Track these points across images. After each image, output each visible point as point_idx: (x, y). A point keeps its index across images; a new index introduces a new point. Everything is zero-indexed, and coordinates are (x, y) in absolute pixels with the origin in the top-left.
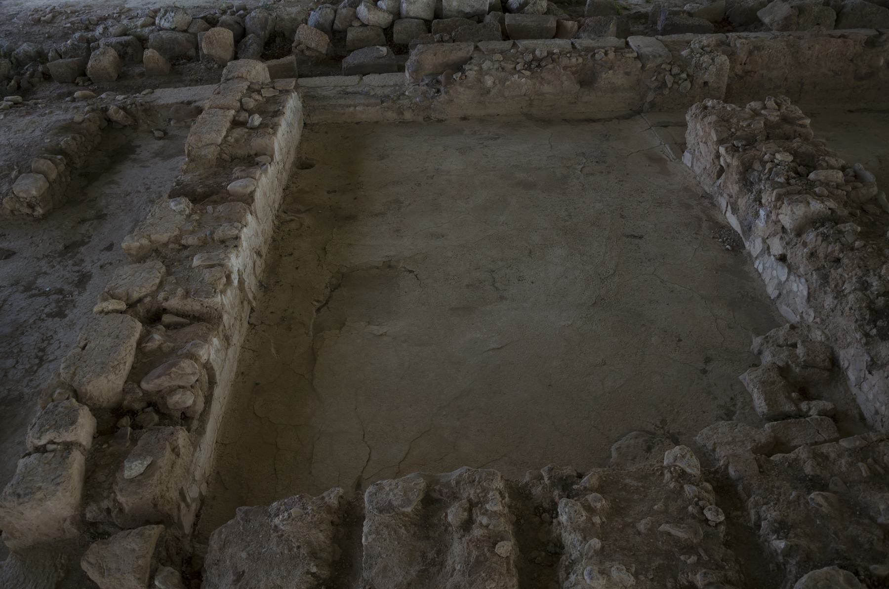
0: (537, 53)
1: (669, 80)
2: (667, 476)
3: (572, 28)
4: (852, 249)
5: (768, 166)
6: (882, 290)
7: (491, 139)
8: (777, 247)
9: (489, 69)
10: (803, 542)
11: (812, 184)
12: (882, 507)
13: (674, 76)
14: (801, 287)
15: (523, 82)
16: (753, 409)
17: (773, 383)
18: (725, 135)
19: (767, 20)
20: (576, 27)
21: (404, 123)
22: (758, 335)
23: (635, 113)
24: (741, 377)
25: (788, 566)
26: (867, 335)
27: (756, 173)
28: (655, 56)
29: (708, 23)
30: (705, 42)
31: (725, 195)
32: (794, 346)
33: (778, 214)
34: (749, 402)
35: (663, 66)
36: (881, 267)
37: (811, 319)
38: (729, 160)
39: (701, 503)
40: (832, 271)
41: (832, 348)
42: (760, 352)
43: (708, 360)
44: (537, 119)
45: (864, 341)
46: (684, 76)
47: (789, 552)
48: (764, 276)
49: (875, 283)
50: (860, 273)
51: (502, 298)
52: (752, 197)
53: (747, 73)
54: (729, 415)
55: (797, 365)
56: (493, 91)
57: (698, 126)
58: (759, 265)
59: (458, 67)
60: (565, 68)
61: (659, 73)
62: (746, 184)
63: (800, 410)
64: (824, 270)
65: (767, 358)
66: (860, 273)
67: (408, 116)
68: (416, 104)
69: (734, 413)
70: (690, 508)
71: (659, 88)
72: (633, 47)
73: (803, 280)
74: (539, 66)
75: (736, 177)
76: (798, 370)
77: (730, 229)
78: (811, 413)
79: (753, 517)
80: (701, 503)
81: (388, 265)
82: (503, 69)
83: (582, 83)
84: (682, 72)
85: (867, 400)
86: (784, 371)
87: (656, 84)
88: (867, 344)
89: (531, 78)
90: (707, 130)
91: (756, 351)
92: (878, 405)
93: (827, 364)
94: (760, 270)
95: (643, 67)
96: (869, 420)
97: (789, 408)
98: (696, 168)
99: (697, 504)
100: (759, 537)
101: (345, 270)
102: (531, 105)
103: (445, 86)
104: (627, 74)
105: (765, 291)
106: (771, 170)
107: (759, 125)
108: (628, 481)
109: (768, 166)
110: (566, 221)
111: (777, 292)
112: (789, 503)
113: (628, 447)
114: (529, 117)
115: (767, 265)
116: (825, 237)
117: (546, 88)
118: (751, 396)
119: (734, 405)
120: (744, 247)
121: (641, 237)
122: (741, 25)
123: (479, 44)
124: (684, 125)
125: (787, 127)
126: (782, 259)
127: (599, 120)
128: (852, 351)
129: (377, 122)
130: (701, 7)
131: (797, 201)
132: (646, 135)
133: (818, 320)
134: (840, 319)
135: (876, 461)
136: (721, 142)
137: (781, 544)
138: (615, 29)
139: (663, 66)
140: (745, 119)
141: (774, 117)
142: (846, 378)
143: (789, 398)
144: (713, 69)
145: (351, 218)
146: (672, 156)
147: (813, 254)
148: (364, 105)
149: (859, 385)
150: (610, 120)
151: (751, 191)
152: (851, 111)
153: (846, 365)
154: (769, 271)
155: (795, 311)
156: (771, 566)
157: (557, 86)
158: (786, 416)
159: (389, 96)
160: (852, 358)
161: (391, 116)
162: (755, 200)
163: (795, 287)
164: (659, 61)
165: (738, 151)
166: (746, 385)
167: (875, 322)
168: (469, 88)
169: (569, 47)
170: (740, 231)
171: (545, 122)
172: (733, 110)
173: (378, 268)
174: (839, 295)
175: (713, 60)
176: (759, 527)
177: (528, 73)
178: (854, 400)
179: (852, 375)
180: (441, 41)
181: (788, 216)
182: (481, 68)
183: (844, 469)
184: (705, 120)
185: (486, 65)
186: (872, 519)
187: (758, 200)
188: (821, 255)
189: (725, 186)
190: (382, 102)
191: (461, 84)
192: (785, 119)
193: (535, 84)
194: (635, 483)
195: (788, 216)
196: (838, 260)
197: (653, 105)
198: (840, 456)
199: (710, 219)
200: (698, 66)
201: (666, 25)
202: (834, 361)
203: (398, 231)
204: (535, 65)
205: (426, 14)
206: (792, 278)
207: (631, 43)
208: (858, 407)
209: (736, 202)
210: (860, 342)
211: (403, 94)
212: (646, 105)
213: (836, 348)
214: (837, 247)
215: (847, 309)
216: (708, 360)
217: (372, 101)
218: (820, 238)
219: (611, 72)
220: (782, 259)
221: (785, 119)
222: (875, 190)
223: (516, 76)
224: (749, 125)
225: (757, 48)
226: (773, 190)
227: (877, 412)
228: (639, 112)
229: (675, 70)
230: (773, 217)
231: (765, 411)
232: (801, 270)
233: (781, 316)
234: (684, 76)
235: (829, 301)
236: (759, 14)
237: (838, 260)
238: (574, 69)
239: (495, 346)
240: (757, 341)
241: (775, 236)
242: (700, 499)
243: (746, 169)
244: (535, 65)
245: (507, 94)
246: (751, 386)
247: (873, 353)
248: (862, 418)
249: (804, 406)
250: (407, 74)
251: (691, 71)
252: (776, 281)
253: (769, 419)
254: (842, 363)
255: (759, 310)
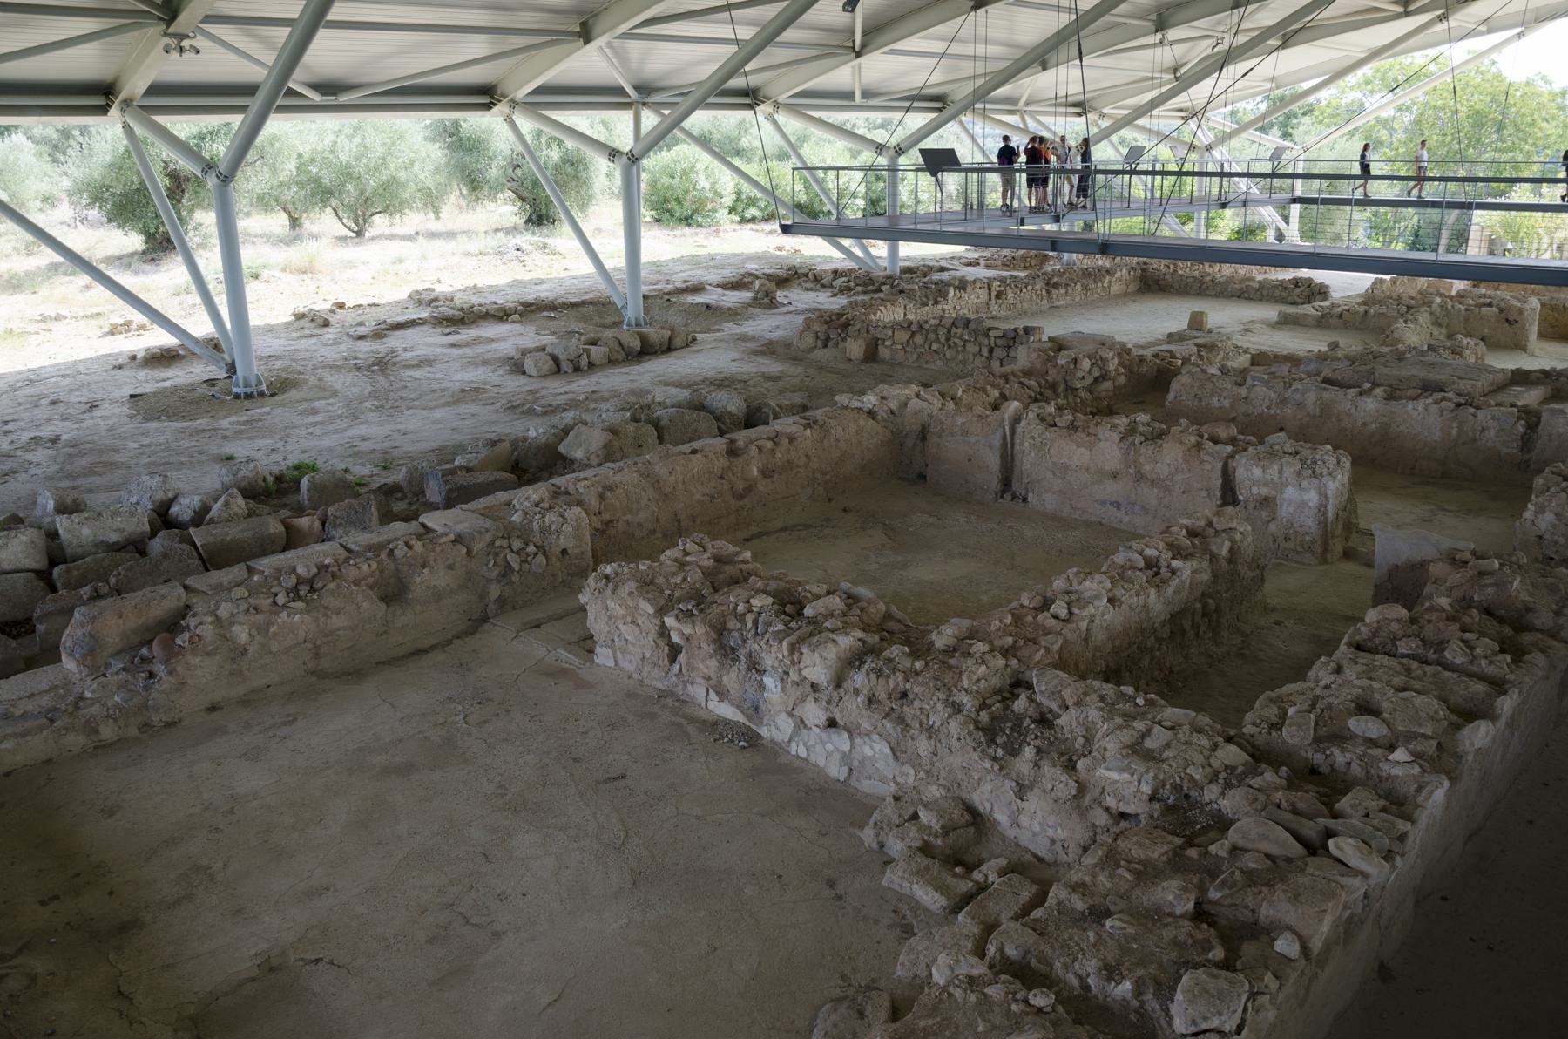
0: (300, 570)
1: (514, 560)
2: (958, 993)
3: (311, 526)
4: (917, 673)
5: (749, 618)
6: (977, 703)
7: (284, 724)
8: (814, 713)
9: (232, 615)
10: (1141, 972)
11: (813, 621)
12: (1171, 898)
13: (517, 553)
14: (877, 747)
15: (297, 621)
16: (926, 910)
17: (928, 869)
18: (662, 602)
19: (579, 454)
20: (317, 524)
21: (104, 748)
22: (862, 828)
23: (479, 622)
24: (884, 883)
25: (1147, 1006)
26: (995, 759)
27: (736, 634)
28: (480, 533)
29: (505, 475)
30: (535, 497)
31: (698, 680)
32: (915, 817)
33: (800, 671)
34: (916, 906)
35: (498, 543)
36: (960, 679)
37: (912, 779)
38: (687, 630)
39: (1018, 996)
40: (905, 708)
41: (959, 797)
42: (882, 845)
43: (831, 884)
44: (337, 673)
45: (996, 767)
46: (531, 549)
47: (1138, 992)
48: (813, 759)
49: (967, 702)
50: (942, 696)
51: (497, 935)
52: (743, 667)
53: (608, 523)
54: (908, 931)
55: (936, 837)
56: (251, 649)
57: (611, 604)
58: (797, 749)
59: (173, 625)
60: (356, 583)
61: (497, 554)
62: (726, 652)
63: (977, 883)
64: (893, 708)
65: (895, 846)
66: (942, 696)
67: (107, 732)
68: (117, 706)
69: (912, 926)
70: (1014, 1007)
71: (504, 575)
72: (435, 527)
73: (875, 737)
74: (312, 590)
75: (708, 648)
76: (939, 842)
77: (727, 722)
78: (991, 880)
79: (1075, 982)
80: (1018, 996)
81: (270, 967)
82: (256, 609)
83: (387, 599)
84: (527, 544)
85: (1034, 834)
86: (926, 850)
87: (496, 572)
88: (1001, 769)
89: (308, 612)
90: (630, 603)
91: (875, 846)
92: (1050, 832)
93: (968, 817)
94: (802, 752)
95: (469, 552)
96: (1048, 857)
97: (964, 886)
98: (624, 665)
99: (1016, 1000)
100: (1096, 997)
101: (191, 1010)
102: (317, 656)
103: (167, 662)
104: (450, 567)
105: (827, 776)
106: (755, 623)
107: (695, 576)
108: (922, 1023)
109: (749, 618)
110: (503, 796)
111: (846, 769)
112: (1094, 945)
113: (835, 1026)
114: (321, 674)
115: (811, 742)
116: (879, 673)
117: (337, 621)
118: (912, 898)
119: (904, 917)
120: (759, 736)
121: (624, 777)
122: (541, 470)
123: (188, 582)
124: (583, 609)
125: (728, 569)
126: (832, 723)
127: (433, 648)
128: (987, 787)
129: (49, 761)
130: (481, 457)
131: (819, 643)
132: (514, 648)
133: (922, 774)
134: (951, 759)
135: (1129, 862)
136: (661, 612)
137: (1127, 986)
138: (1503, 286)
139: (498, 543)
140: (674, 574)
141: (708, 562)
142: (995, 823)
143: (955, 875)
144: (567, 528)
145: (127, 927)
146: (576, 661)
147: (871, 701)
148: (15, 735)
149: (1015, 822)
150: (449, 642)
151: (737, 659)
152: (747, 540)
153: (988, 807)
154: (819, 749)
155: (883, 780)
156: (1132, 1017)
157: (351, 613)
158: (967, 899)
159: (55, 709)
160: (992, 796)
161: (75, 741)
162: (749, 670)
163: (868, 751)
164: (488, 537)
165: (692, 615)
166: (897, 888)
167: (993, 741)
168: (208, 654)
169: (342, 553)
170: (741, 718)
171: (353, 674)
172: (650, 567)
173: (253, 980)
174: (931, 732)
175: (562, 516)
176: (1087, 988)
177: (300, 605)
178: (1017, 845)
179: (1001, 817)
180: (97, 596)
181: (817, 666)
182: (217, 618)
183: (1109, 885)
184: (619, 591)
185: (224, 611)
186: (1171, 915)
187: (755, 667)
188: (883, 696)
189: (691, 668)
190: (52, 721)
191: (194, 652)
192: (719, 559)
193: (317, 620)
194: (930, 1022)
195: (817, 666)
196: (904, 695)
197: (502, 602)
198: (1094, 876)
199: (692, 720)
200: (545, 531)
201: (449, 491)
202: (971, 810)
203: (239, 911)
204: (306, 589)
205: (36, 561)
206: (858, 741)
207: (430, 525)
208: (1027, 850)
209: (720, 682)
210: (988, 772)
211: (81, 698)
212: (491, 606)
213: (964, 795)
214: (900, 677)
215: (954, 742)
216: (831, 884)
217: (30, 724)
218: (873, 676)
219: (426, 571)
220: (832, 723)
221: (719, 559)
222: (882, 606)
223: (284, 615)
224: (684, 579)
225: (610, 488)
226: (780, 642)
227: (1053, 842)
228: (485, 619)
229: (517, 544)
230: (794, 676)
231: (944, 903)
232: (866, 725)
233: (867, 795)
234: (531, 549)
235: (923, 746)
236: (561, 449)
237: (904, 695)
238: (371, 580)
239: (545, 1001)
240: (868, 835)
241: (803, 700)
242: (1015, 994)
243: (720, 632)
244: (306, 589)
245: (275, 647)
246: (906, 884)
247: (1014, 775)
248: (1041, 860)
249: (977, 876)
250: (68, 663)
251: (537, 540)
252: (837, 756)
253: (956, 909)
254: (981, 809)
255: (836, 802)
